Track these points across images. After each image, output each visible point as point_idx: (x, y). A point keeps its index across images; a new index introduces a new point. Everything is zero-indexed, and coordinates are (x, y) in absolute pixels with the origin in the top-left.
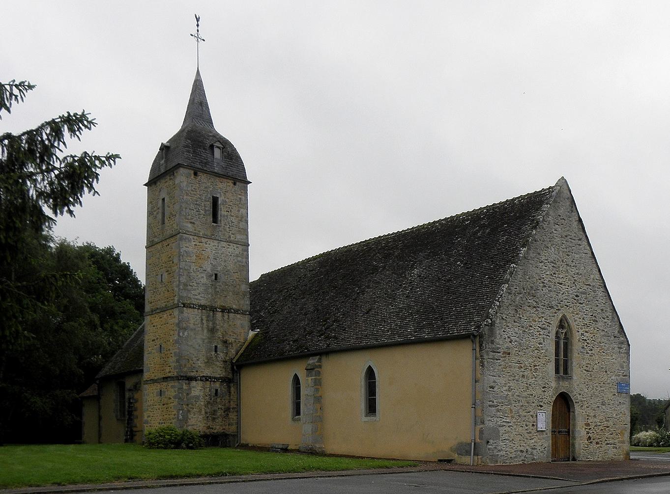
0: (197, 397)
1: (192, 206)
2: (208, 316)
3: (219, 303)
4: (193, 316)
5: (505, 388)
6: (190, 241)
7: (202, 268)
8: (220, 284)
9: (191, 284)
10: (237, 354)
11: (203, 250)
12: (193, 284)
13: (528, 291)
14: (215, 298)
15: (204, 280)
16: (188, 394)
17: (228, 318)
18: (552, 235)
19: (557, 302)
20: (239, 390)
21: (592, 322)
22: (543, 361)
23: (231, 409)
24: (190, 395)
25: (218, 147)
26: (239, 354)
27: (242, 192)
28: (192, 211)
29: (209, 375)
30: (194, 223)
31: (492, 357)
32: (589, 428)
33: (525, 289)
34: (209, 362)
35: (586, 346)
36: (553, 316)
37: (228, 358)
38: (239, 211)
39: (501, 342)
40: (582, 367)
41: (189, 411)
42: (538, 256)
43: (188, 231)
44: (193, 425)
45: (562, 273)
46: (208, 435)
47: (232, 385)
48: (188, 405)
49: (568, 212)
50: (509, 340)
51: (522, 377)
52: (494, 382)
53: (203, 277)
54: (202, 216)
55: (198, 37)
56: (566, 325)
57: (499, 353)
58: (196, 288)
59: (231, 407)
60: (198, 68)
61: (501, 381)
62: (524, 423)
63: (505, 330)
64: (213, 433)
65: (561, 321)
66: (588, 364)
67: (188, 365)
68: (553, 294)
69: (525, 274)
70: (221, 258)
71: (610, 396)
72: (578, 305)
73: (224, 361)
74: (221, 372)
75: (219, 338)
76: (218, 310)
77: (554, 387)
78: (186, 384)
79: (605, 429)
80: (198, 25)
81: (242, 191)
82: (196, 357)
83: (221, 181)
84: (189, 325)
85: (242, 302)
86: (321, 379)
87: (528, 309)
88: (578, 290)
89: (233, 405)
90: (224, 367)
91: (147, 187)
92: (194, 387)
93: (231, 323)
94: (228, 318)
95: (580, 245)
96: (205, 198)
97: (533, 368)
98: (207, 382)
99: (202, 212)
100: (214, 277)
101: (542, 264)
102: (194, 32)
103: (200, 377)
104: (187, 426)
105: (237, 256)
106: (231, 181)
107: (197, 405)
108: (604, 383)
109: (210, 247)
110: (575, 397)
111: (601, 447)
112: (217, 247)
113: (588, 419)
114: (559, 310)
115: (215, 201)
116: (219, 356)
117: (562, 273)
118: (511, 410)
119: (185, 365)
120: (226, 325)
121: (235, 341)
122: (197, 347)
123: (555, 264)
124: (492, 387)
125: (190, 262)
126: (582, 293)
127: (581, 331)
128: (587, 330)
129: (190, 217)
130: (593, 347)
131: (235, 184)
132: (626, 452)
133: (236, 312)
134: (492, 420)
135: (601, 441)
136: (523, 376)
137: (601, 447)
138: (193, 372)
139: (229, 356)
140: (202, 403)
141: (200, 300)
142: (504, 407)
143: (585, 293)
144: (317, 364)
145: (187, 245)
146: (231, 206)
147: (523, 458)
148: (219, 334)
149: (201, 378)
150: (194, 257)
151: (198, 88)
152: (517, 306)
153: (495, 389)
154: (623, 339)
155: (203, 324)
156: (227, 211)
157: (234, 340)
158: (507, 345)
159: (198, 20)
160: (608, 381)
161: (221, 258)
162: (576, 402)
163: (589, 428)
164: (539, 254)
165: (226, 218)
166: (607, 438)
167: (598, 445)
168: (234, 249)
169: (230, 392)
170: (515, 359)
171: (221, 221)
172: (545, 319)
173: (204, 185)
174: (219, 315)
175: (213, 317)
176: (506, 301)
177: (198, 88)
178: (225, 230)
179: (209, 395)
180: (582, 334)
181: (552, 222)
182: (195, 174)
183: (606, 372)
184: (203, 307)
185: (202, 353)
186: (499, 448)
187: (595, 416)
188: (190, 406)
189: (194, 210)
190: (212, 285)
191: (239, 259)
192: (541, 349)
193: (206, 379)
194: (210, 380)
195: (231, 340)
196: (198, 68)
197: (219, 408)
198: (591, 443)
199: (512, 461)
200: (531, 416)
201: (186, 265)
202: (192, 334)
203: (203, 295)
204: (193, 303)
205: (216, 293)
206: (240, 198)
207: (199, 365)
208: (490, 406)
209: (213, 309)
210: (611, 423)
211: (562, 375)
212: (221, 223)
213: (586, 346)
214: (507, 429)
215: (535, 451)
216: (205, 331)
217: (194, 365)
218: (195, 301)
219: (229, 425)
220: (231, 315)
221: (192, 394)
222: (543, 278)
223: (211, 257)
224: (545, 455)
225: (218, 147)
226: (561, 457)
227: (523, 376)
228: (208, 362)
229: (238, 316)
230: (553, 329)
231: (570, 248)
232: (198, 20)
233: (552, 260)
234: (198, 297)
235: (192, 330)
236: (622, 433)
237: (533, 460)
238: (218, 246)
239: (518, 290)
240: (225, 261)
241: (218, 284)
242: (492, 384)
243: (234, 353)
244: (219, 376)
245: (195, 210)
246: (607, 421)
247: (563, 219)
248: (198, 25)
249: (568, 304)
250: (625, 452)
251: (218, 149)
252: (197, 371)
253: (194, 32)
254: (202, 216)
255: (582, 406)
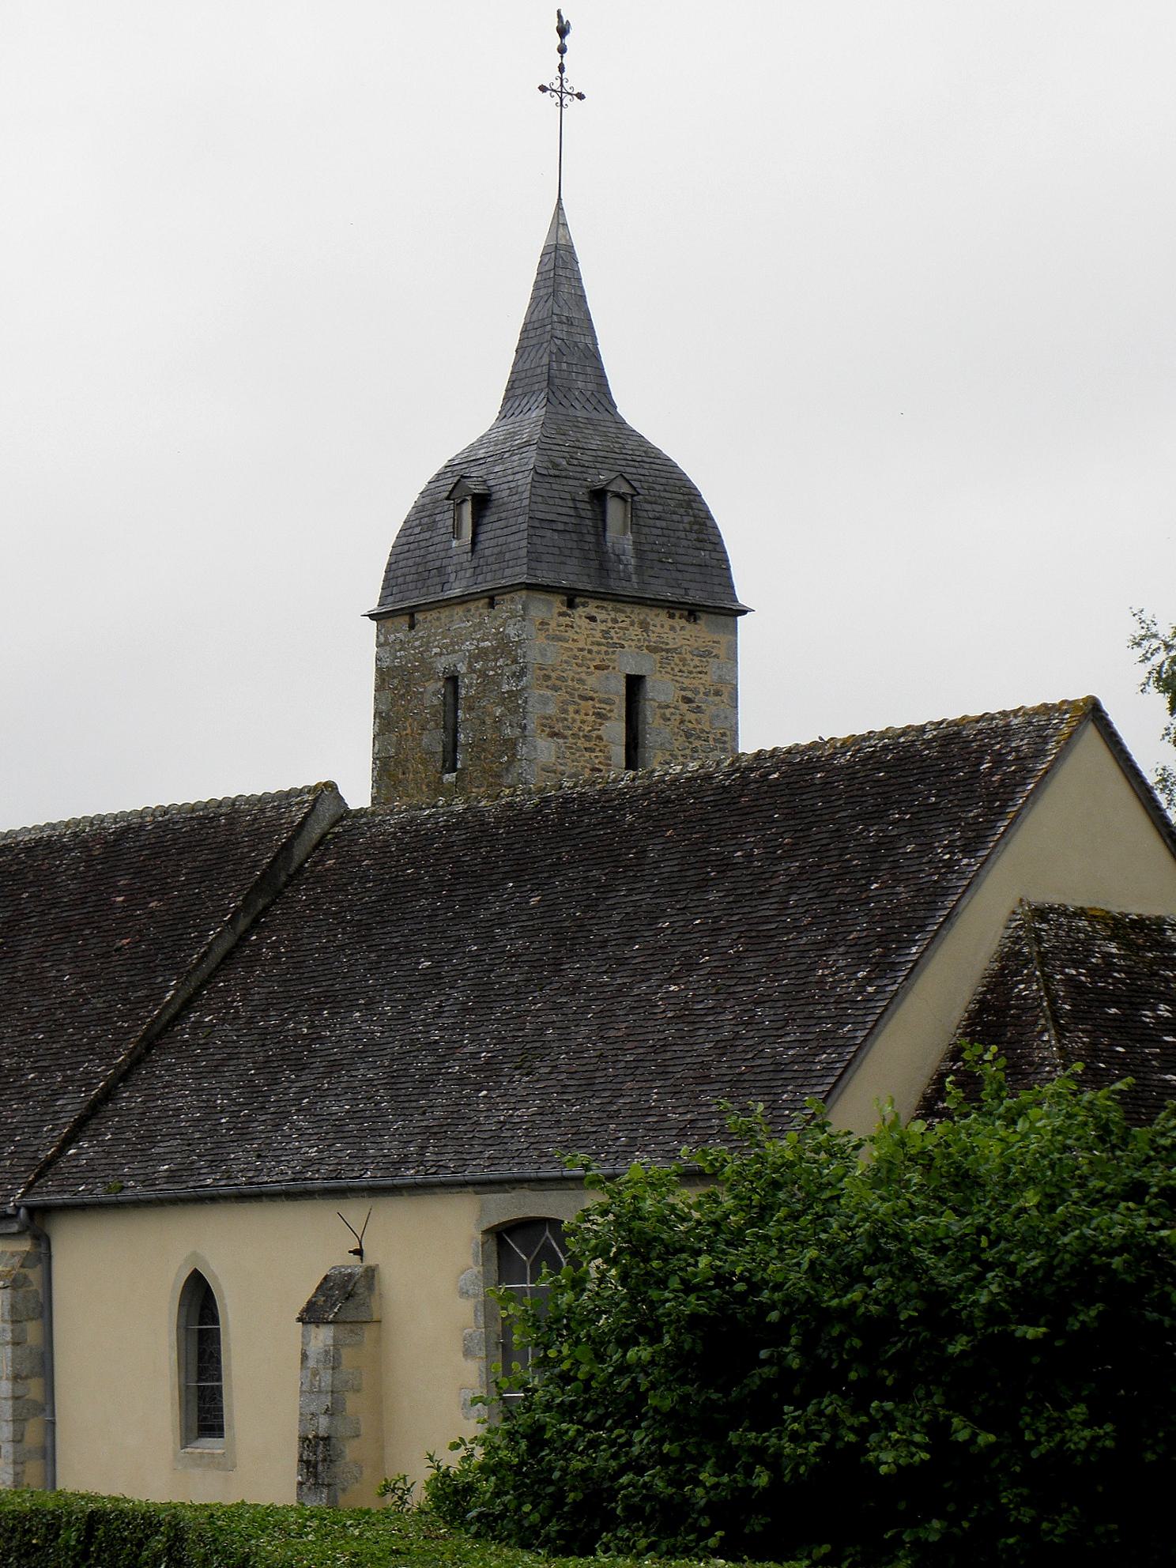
25: (618, 495)
55: (561, 92)
60: (560, 198)
77: (568, 40)
80: (562, 50)
91: (375, 622)
102: (550, 78)
151: (559, 220)
159: (563, 31)
177: (559, 220)
196: (560, 198)
225: (618, 495)
232: (563, 31)
248: (562, 50)
251: (617, 500)
253: (550, 78)
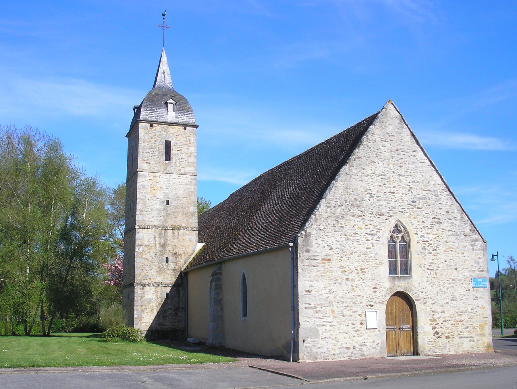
0: (150, 300)
1: (148, 150)
2: (160, 234)
3: (170, 222)
4: (147, 235)
5: (324, 291)
6: (145, 177)
7: (155, 196)
8: (171, 208)
9: (146, 210)
10: (185, 263)
11: (157, 183)
12: (148, 209)
13: (351, 203)
14: (167, 219)
15: (158, 206)
16: (142, 297)
17: (178, 235)
18: (379, 151)
19: (388, 209)
20: (186, 291)
21: (434, 223)
22: (372, 263)
23: (180, 309)
24: (144, 298)
26: (187, 263)
27: (191, 134)
28: (148, 154)
29: (160, 281)
30: (149, 163)
31: (308, 264)
32: (435, 323)
33: (348, 201)
34: (160, 271)
35: (428, 246)
36: (383, 223)
37: (177, 267)
38: (188, 149)
39: (319, 251)
40: (424, 267)
41: (143, 311)
42: (362, 171)
43: (144, 169)
44: (146, 322)
45: (394, 182)
46: (160, 330)
47: (181, 289)
48: (142, 306)
49: (398, 129)
50: (329, 248)
51: (346, 280)
52: (311, 286)
53: (156, 204)
54: (157, 156)
56: (402, 229)
57: (317, 260)
58: (151, 212)
59: (180, 307)
61: (321, 284)
62: (350, 322)
63: (323, 240)
64: (164, 328)
65: (396, 225)
66: (432, 263)
67: (142, 274)
68: (384, 203)
69: (347, 188)
70: (172, 187)
71: (463, 291)
72: (415, 209)
73: (174, 270)
74: (171, 278)
75: (170, 251)
76: (169, 228)
78: (140, 289)
79: (458, 324)
81: (191, 133)
82: (149, 267)
83: (173, 128)
84: (143, 242)
85: (191, 220)
86: (221, 284)
87: (352, 218)
88: (415, 196)
89: (181, 305)
90: (173, 275)
92: (147, 292)
93: (180, 238)
94: (178, 235)
95: (415, 156)
96: (159, 142)
97: (360, 272)
98: (159, 287)
99: (157, 154)
100: (166, 203)
101: (369, 177)
103: (153, 283)
104: (141, 323)
105: (186, 185)
106: (182, 127)
107: (150, 306)
108: (453, 280)
109: (163, 179)
110: (416, 295)
111: (453, 341)
112: (168, 179)
113: (434, 315)
114: (391, 216)
115: (168, 145)
116: (170, 265)
117: (394, 182)
118: (333, 311)
119: (140, 275)
120: (176, 240)
121: (184, 253)
122: (150, 259)
123: (385, 175)
124: (309, 291)
125: (146, 193)
126: (420, 199)
127: (420, 234)
128: (429, 232)
129: (146, 159)
130: (437, 247)
131: (185, 129)
132: (487, 344)
133: (185, 229)
134: (309, 321)
135: (452, 335)
136: (347, 279)
137: (453, 341)
138: (146, 279)
139: (178, 265)
140: (154, 305)
141: (153, 222)
142: (324, 308)
143: (423, 198)
144: (217, 272)
145: (143, 180)
146: (181, 146)
147: (349, 354)
148: (170, 248)
149: (153, 284)
150: (150, 189)
152: (337, 217)
153: (312, 293)
154: (476, 236)
155: (155, 240)
156: (178, 150)
157: (183, 252)
158: (326, 252)
160: (460, 278)
161: (172, 187)
162: (416, 300)
163: (435, 323)
164: (364, 169)
165: (177, 155)
166: (460, 332)
167: (448, 340)
168: (184, 179)
169: (179, 295)
170: (334, 263)
171: (172, 158)
172: (373, 226)
173: (158, 133)
174: (170, 232)
175: (165, 234)
176: (323, 214)
178: (176, 165)
179: (161, 298)
180: (422, 236)
181: (378, 140)
182: (152, 126)
183: (456, 269)
184: (156, 227)
185: (154, 264)
186: (319, 346)
187: (443, 312)
188: (144, 307)
189: (149, 153)
190: (164, 209)
191: (188, 186)
192: (369, 253)
193: (158, 285)
194: (161, 285)
195: (180, 251)
197: (169, 309)
198: (439, 337)
199: (336, 357)
200: (359, 315)
201: (142, 196)
202: (146, 249)
203: (156, 218)
204: (148, 224)
205: (168, 215)
206: (190, 139)
207: (152, 273)
208: (306, 308)
209: (165, 229)
210: (465, 317)
211: (400, 275)
212: (172, 160)
213: (428, 246)
214: (328, 328)
215: (364, 348)
216: (158, 246)
217: (147, 274)
218: (149, 222)
219: (178, 322)
220: (181, 232)
221: (145, 297)
222: (370, 190)
223: (164, 187)
224: (378, 351)
226: (403, 352)
227: (347, 279)
228: (159, 271)
229: (187, 232)
230: (385, 236)
231: (403, 160)
233: (381, 173)
234: (152, 219)
235: (146, 246)
236: (482, 327)
237: (362, 356)
238: (170, 178)
239: (338, 203)
240: (176, 189)
241: (170, 208)
242: (308, 288)
243: (183, 262)
244: (169, 282)
245: (151, 153)
246: (459, 315)
247: (392, 136)
249: (403, 210)
250: (486, 344)
252: (150, 279)
254: (157, 156)
255: (425, 303)
